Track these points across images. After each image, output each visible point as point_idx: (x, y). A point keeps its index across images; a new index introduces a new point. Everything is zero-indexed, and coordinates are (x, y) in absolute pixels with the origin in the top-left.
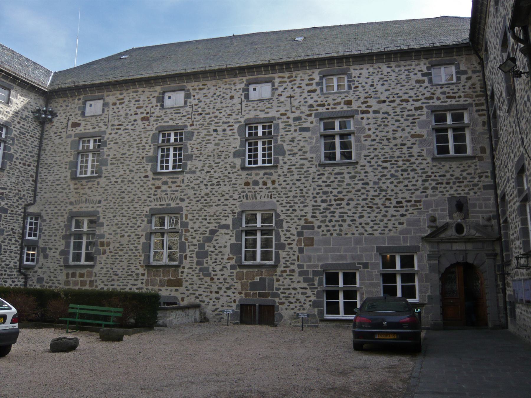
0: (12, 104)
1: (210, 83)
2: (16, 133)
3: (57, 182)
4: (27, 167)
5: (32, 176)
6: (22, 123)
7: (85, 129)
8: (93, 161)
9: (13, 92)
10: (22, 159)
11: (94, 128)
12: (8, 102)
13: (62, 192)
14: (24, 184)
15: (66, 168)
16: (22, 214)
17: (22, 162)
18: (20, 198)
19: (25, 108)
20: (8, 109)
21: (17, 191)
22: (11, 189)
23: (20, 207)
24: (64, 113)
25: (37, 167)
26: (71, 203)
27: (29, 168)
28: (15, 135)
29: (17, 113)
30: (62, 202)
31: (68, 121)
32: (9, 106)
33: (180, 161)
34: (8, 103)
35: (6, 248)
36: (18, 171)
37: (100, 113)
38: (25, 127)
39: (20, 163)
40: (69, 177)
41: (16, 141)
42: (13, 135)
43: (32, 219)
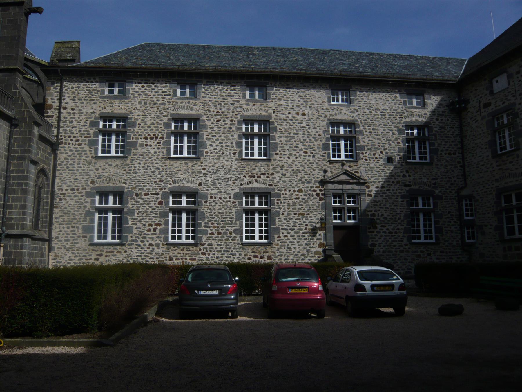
0: (427, 106)
1: (369, 72)
2: (437, 129)
3: (482, 163)
4: (452, 156)
5: (459, 162)
6: (440, 119)
7: (496, 107)
8: (510, 135)
9: (426, 96)
10: (447, 150)
11: (504, 103)
12: (424, 105)
13: (487, 171)
14: (453, 171)
15: (486, 148)
16: (457, 198)
17: (447, 152)
18: (452, 184)
19: (440, 105)
20: (425, 111)
21: (448, 179)
22: (442, 178)
23: (453, 192)
24: (475, 97)
25: (462, 153)
26: (497, 180)
27: (455, 156)
28: (436, 131)
29: (433, 112)
30: (488, 181)
31: (480, 104)
32: (425, 109)
33: (351, 151)
34: (424, 106)
35: (447, 229)
36: (445, 161)
37: (506, 86)
38: (444, 121)
39: (446, 154)
40: (490, 156)
41: (438, 136)
42: (434, 132)
43: (466, 201)
